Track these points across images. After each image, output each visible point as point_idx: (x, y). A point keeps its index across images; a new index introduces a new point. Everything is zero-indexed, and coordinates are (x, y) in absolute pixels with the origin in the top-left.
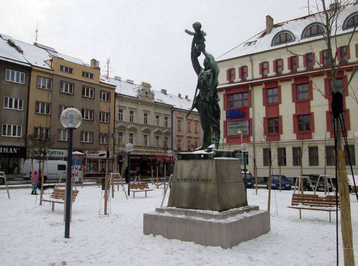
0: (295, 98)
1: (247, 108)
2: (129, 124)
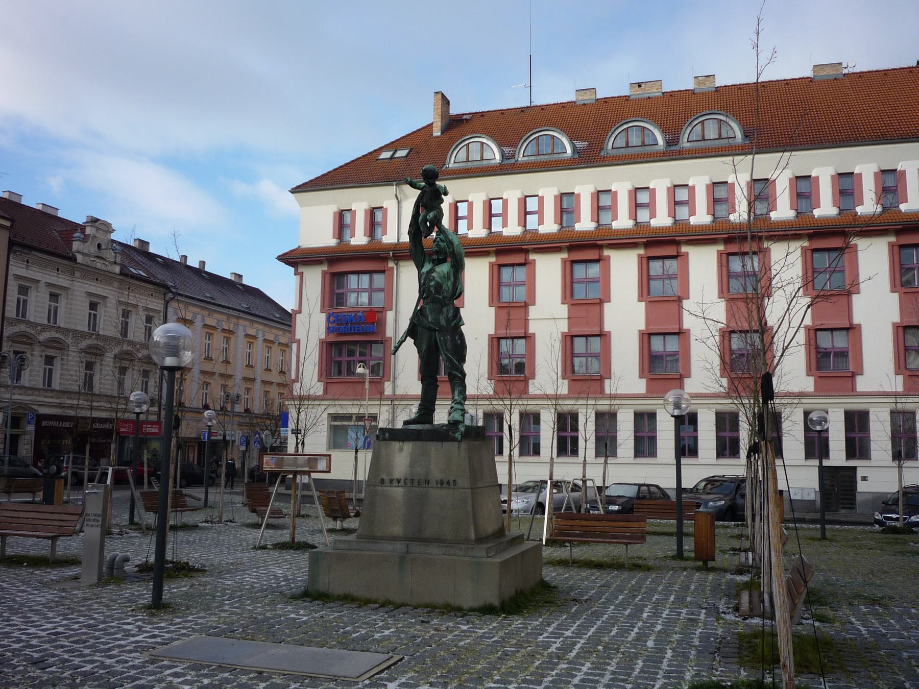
0: (495, 295)
2: (44, 328)
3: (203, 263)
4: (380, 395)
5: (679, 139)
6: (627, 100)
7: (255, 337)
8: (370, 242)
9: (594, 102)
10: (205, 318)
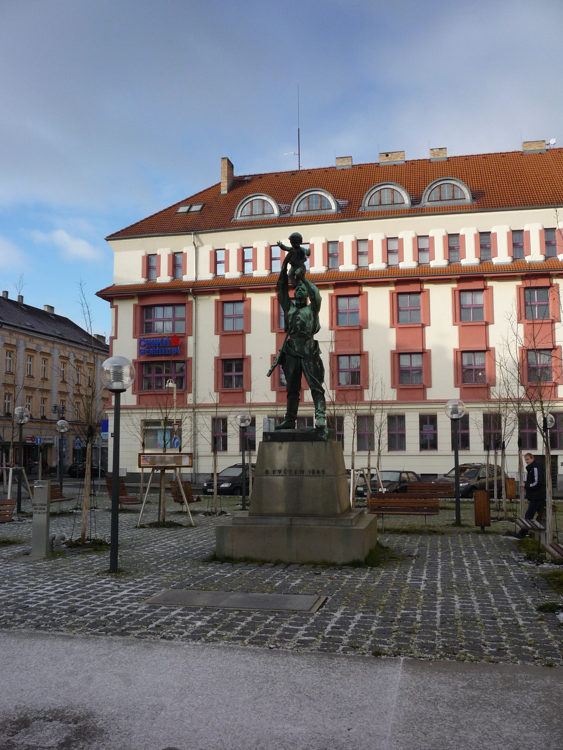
1: (184, 337)
3: (21, 297)
4: (182, 404)
5: (421, 199)
6: (377, 166)
7: (67, 358)
8: (172, 280)
9: (351, 167)
10: (27, 343)
